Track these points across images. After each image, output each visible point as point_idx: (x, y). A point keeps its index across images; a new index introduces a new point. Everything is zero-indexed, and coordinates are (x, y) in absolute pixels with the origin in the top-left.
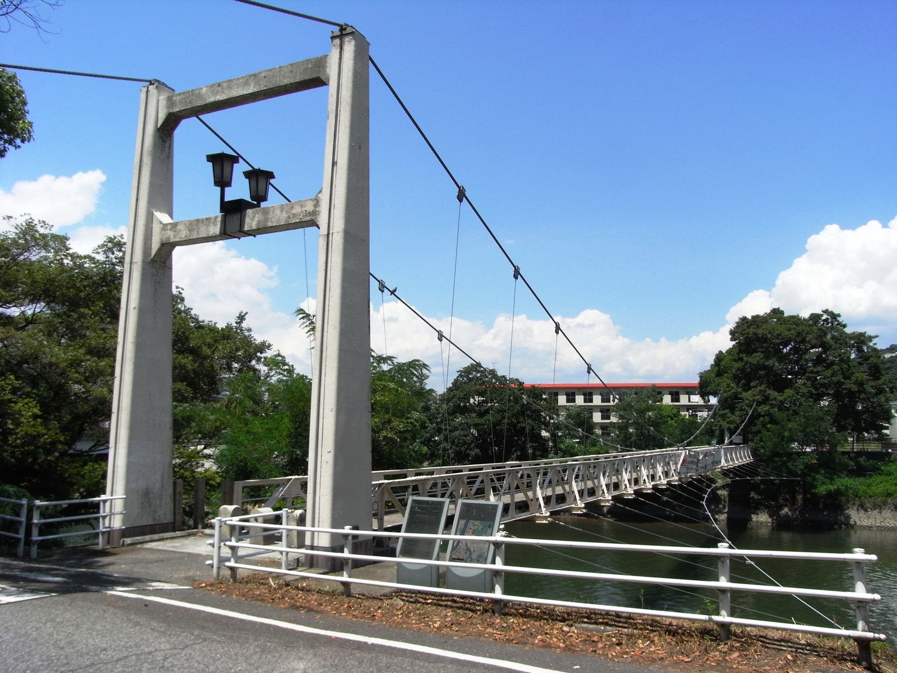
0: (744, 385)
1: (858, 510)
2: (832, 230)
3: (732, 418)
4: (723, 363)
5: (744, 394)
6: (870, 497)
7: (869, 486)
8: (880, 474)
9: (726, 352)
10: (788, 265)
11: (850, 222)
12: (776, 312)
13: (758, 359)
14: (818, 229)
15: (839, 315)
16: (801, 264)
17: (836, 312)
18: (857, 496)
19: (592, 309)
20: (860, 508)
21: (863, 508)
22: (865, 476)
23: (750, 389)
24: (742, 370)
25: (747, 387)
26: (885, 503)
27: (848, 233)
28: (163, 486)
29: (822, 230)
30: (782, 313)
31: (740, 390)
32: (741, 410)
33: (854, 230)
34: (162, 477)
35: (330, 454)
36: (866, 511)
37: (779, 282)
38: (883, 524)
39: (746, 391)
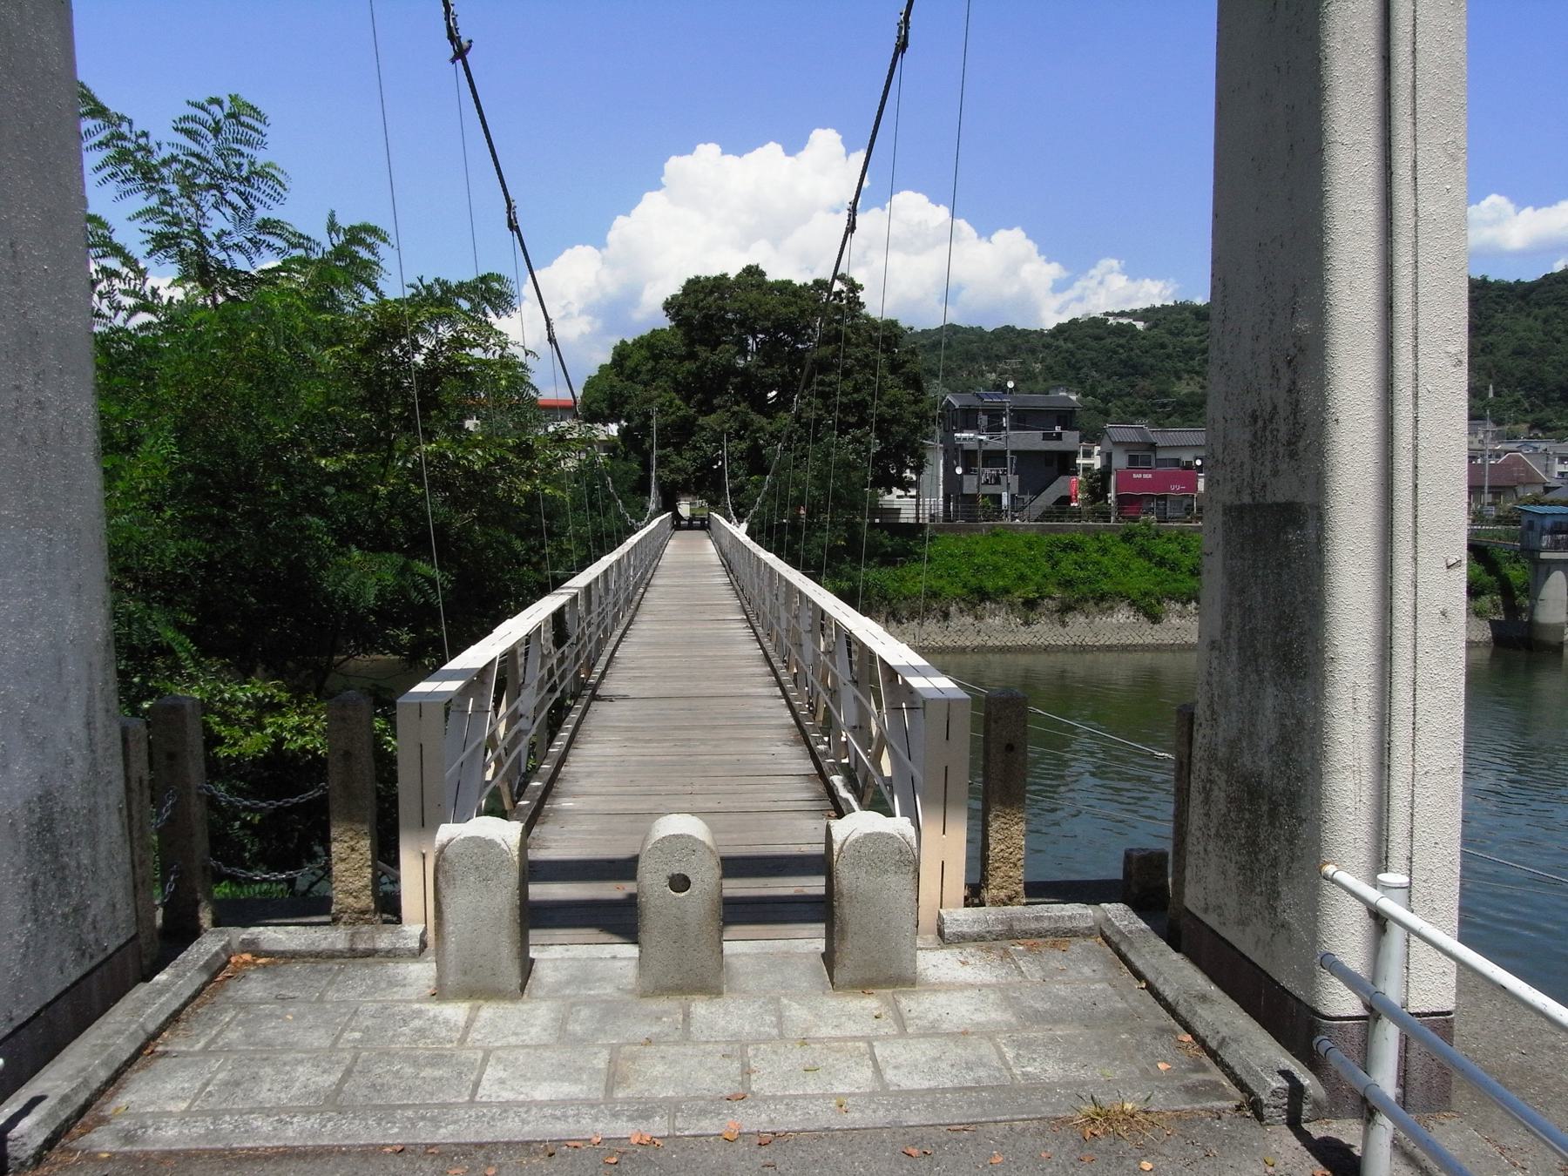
0: (700, 404)
1: (887, 621)
2: (708, 152)
3: (680, 463)
4: (629, 363)
5: (701, 421)
6: (905, 598)
7: (902, 579)
8: (915, 560)
9: (634, 344)
10: (627, 205)
11: (737, 145)
12: (752, 272)
13: (727, 355)
14: (687, 149)
15: (861, 287)
16: (652, 203)
17: (858, 282)
18: (885, 598)
19: (917, 191)
20: (891, 618)
21: (894, 616)
22: (894, 564)
23: (712, 410)
24: (697, 375)
25: (707, 408)
26: (928, 609)
27: (731, 160)
28: (93, 765)
29: (762, 146)
30: (762, 274)
31: (692, 411)
32: (695, 448)
33: (740, 155)
34: (89, 725)
35: (1452, 573)
36: (900, 622)
37: (612, 236)
38: (926, 643)
39: (706, 414)
